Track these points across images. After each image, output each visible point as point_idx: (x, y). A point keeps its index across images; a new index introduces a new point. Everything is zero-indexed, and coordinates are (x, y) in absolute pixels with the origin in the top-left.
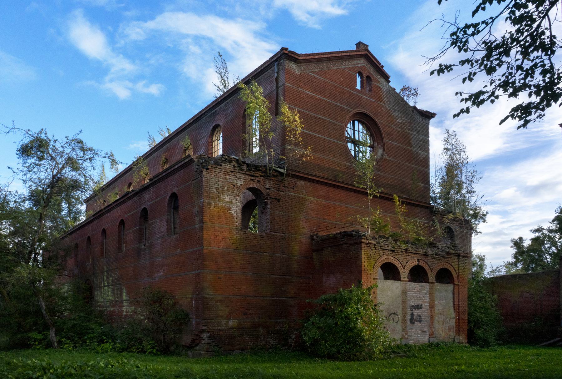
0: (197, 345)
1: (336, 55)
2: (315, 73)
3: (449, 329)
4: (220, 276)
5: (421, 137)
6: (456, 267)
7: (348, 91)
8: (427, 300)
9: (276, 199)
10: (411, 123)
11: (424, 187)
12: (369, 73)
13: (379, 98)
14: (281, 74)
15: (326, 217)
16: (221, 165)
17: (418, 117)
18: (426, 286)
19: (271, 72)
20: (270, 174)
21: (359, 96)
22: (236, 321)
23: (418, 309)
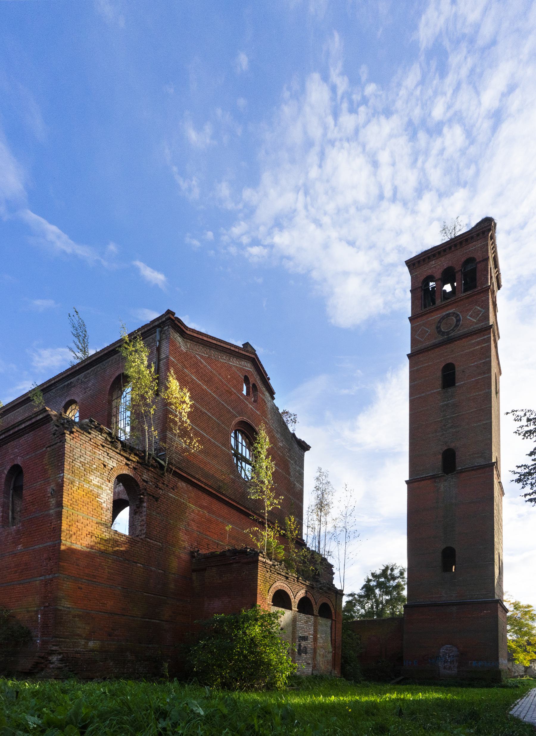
0: (42, 669)
2: (202, 357)
3: (328, 662)
4: (80, 585)
6: (334, 603)
8: (312, 632)
9: (153, 497)
15: (208, 533)
16: (90, 433)
18: (312, 618)
19: (151, 340)
20: (148, 462)
21: (245, 403)
22: (98, 643)
23: (305, 640)
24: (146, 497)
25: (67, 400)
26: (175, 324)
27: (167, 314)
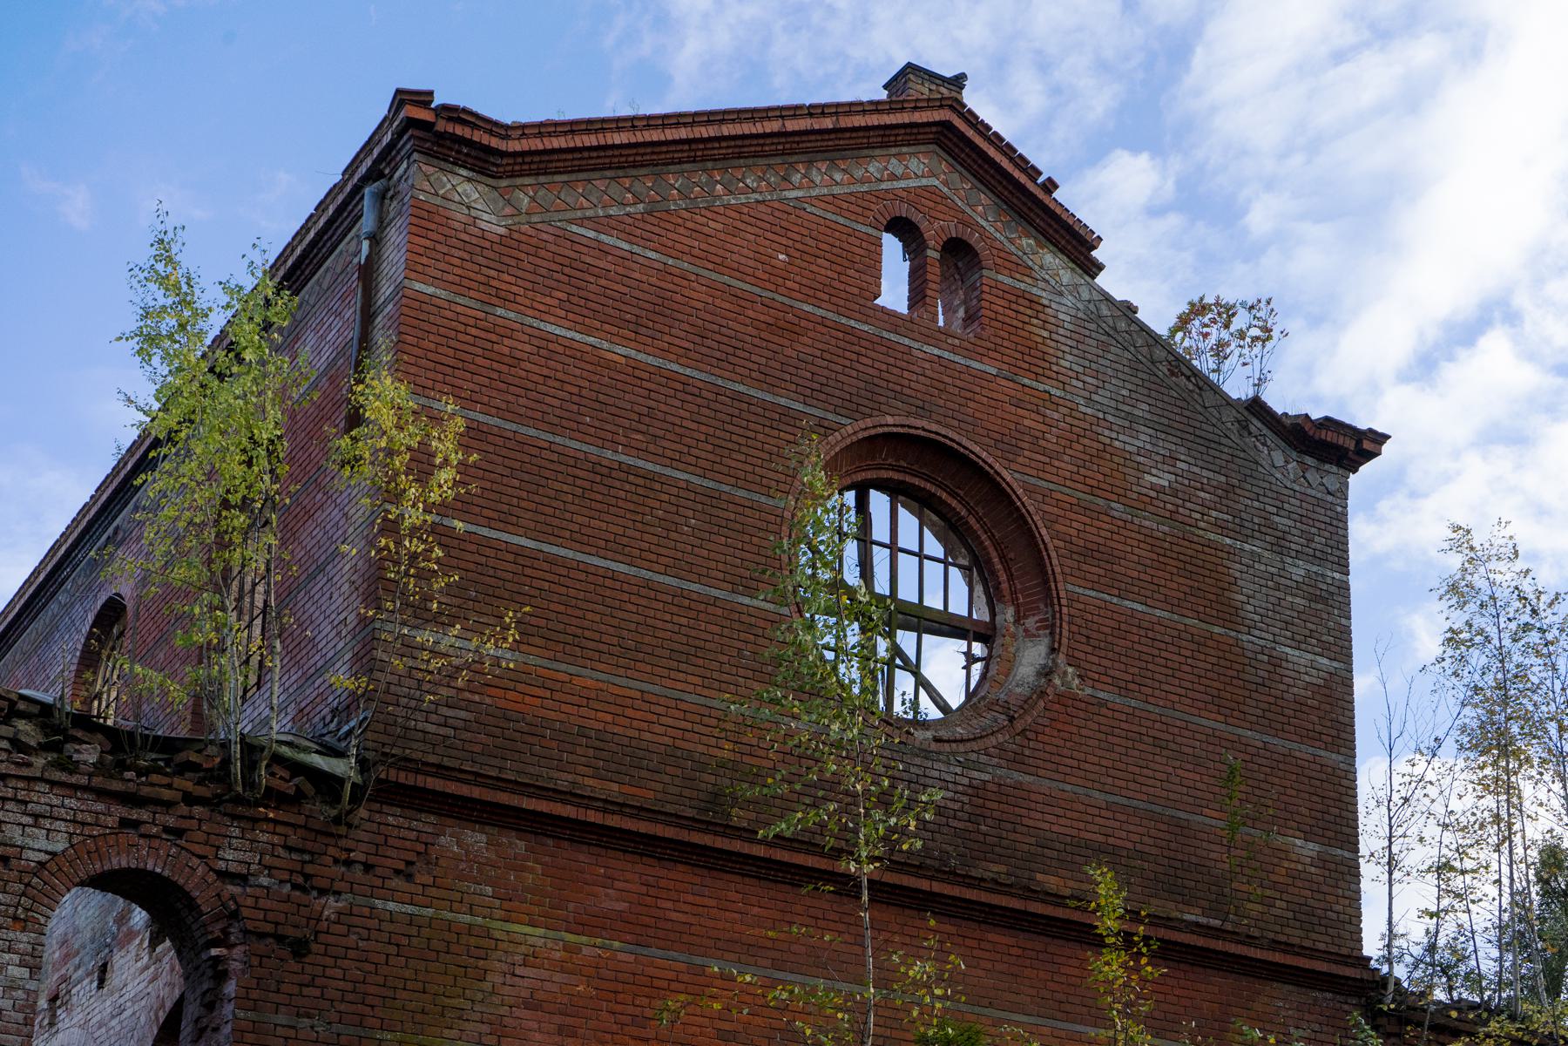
1: (747, 128)
5: (1298, 570)
7: (823, 322)
9: (280, 939)
10: (1229, 489)
11: (1322, 861)
12: (966, 223)
13: (1034, 359)
14: (396, 238)
17: (1277, 458)
20: (249, 784)
21: (891, 347)
24: (238, 952)
25: (100, 603)
26: (442, 136)
27: (397, 111)
